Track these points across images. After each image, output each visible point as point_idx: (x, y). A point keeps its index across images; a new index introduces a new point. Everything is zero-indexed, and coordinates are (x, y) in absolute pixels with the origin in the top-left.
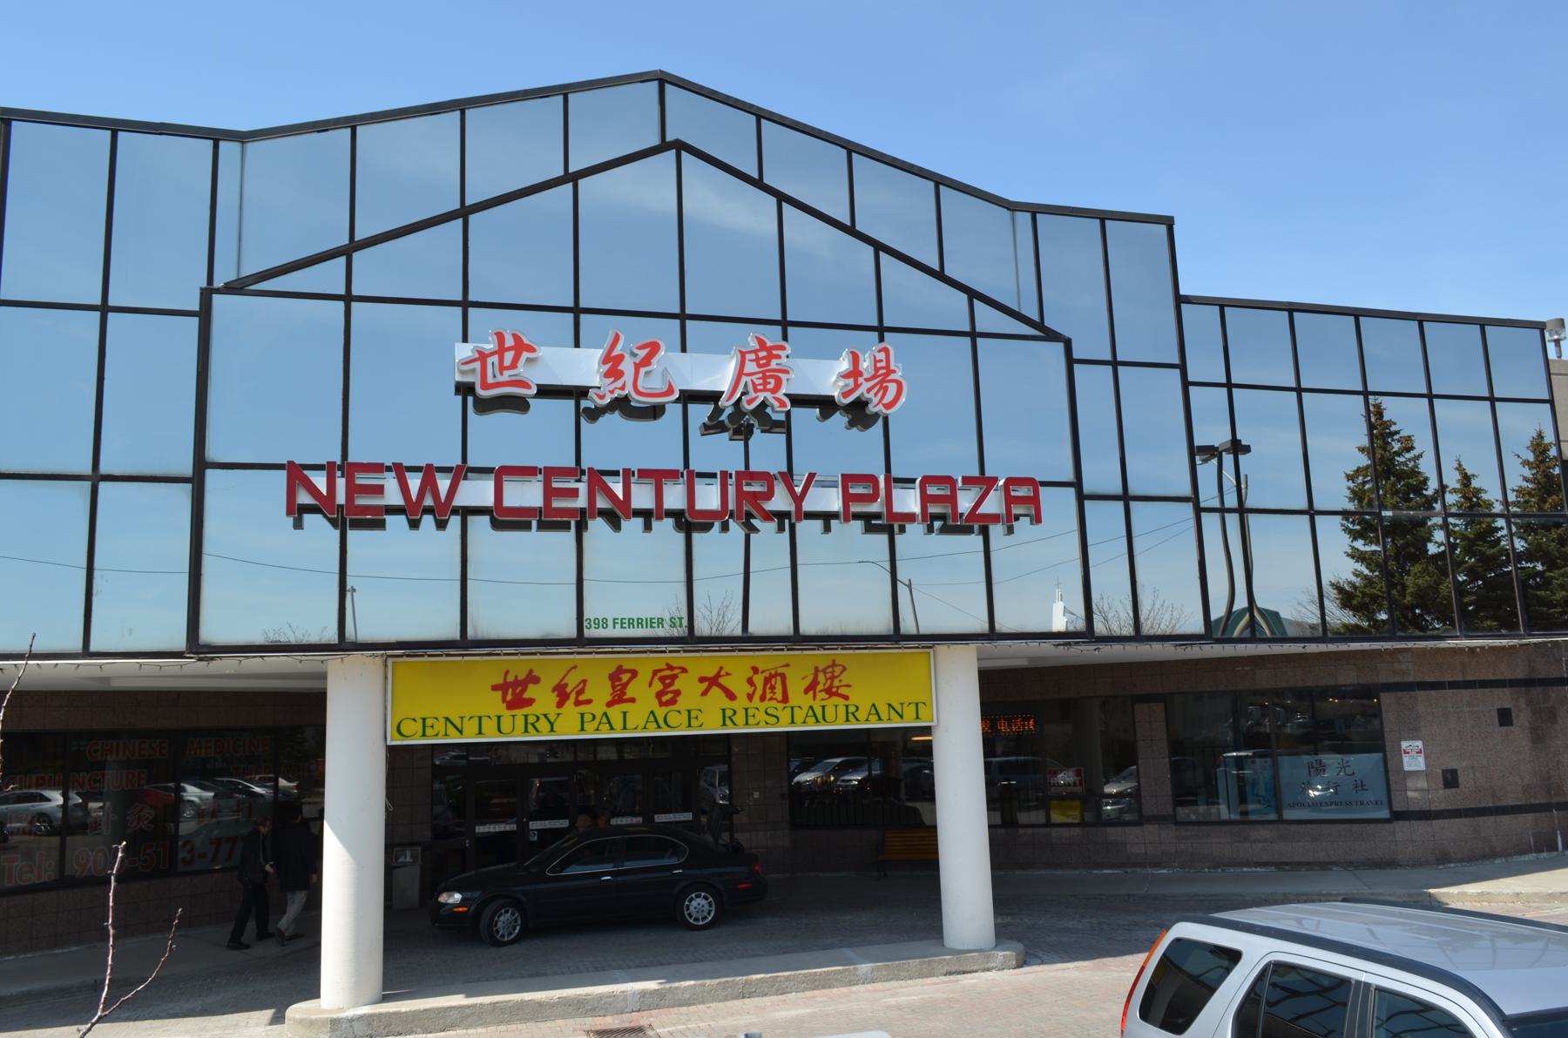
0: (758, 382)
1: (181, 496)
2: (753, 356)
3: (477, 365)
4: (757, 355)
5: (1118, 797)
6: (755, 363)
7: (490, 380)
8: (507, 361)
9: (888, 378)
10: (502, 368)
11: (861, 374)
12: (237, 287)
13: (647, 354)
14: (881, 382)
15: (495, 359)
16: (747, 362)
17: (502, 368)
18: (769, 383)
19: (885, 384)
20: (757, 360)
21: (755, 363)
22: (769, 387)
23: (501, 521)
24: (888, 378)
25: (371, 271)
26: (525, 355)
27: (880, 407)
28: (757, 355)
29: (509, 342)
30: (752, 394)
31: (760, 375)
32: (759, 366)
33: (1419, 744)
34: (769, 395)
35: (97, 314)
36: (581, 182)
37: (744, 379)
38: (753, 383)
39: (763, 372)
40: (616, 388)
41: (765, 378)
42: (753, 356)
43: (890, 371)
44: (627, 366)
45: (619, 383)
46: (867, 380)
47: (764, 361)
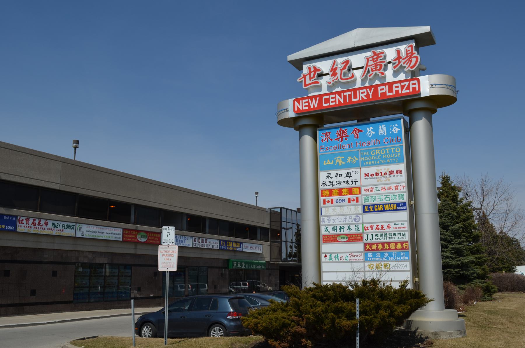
0: (373, 68)
2: (371, 59)
4: (373, 58)
5: (460, 230)
6: (372, 61)
8: (312, 76)
9: (345, 64)
11: (401, 58)
13: (345, 65)
14: (409, 59)
16: (369, 61)
17: (310, 79)
18: (378, 67)
19: (411, 59)
20: (373, 60)
21: (372, 61)
22: (377, 69)
23: (372, 136)
24: (345, 64)
27: (409, 68)
28: (373, 58)
30: (371, 73)
31: (374, 65)
32: (374, 62)
34: (377, 72)
37: (368, 67)
38: (371, 68)
39: (375, 64)
40: (335, 79)
42: (371, 59)
46: (403, 59)
47: (376, 59)
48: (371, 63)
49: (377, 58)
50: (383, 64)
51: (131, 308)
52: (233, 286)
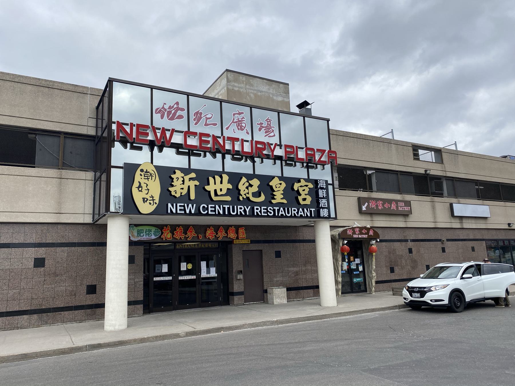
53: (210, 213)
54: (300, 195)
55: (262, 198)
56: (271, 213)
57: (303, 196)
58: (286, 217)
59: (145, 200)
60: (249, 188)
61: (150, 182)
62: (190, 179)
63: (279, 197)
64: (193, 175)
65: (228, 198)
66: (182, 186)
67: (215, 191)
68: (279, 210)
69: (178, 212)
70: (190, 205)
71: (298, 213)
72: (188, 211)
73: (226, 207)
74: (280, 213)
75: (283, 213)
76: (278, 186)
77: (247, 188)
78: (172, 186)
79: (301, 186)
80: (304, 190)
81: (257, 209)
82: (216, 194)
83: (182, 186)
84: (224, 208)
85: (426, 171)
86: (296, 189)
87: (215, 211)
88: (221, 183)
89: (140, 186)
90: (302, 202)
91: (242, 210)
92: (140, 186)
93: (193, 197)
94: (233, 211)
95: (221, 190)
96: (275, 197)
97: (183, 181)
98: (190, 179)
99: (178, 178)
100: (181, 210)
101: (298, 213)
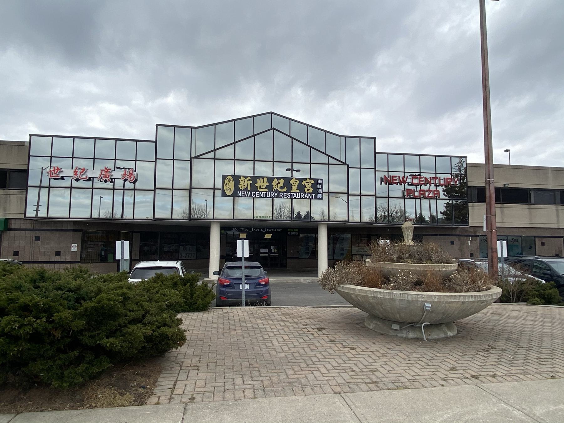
1: (193, 186)
3: (50, 173)
7: (52, 176)
8: (55, 172)
10: (54, 173)
12: (197, 157)
15: (53, 172)
17: (54, 173)
20: (105, 172)
25: (219, 154)
26: (59, 171)
29: (56, 168)
30: (103, 178)
33: (76, 245)
35: (310, 162)
36: (270, 128)
41: (106, 175)
43: (132, 174)
44: (78, 173)
45: (77, 176)
48: (103, 173)
49: (107, 172)
50: (110, 175)
51: (497, 189)
52: (143, 282)
53: (256, 196)
54: (306, 187)
55: (285, 189)
56: (289, 196)
57: (308, 188)
58: (297, 198)
59: (227, 190)
60: (278, 184)
61: (230, 183)
62: (248, 180)
63: (295, 189)
64: (249, 178)
65: (267, 190)
66: (244, 184)
67: (260, 186)
68: (293, 195)
69: (242, 196)
70: (248, 192)
71: (304, 196)
72: (246, 196)
73: (265, 193)
74: (294, 196)
75: (296, 196)
76: (294, 183)
77: (277, 184)
78: (240, 184)
79: (307, 183)
80: (308, 185)
81: (281, 194)
82: (260, 188)
83: (244, 184)
84: (264, 194)
85: (505, 185)
86: (303, 184)
87: (259, 195)
88: (263, 182)
89: (226, 184)
90: (307, 192)
91: (273, 195)
92: (226, 184)
93: (249, 189)
94: (268, 196)
95: (263, 186)
96: (293, 189)
97: (245, 182)
98: (248, 180)
99: (242, 180)
100: (243, 195)
101: (304, 196)
